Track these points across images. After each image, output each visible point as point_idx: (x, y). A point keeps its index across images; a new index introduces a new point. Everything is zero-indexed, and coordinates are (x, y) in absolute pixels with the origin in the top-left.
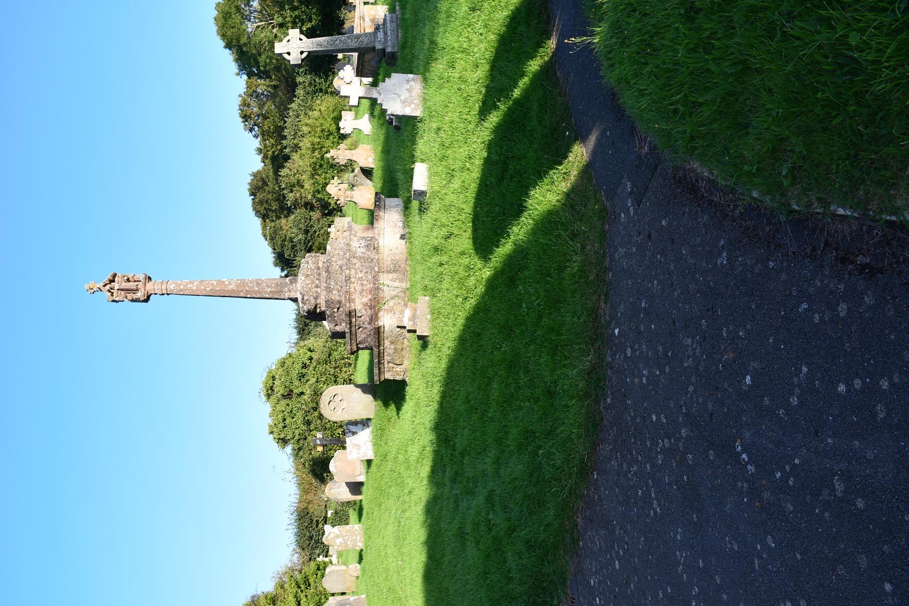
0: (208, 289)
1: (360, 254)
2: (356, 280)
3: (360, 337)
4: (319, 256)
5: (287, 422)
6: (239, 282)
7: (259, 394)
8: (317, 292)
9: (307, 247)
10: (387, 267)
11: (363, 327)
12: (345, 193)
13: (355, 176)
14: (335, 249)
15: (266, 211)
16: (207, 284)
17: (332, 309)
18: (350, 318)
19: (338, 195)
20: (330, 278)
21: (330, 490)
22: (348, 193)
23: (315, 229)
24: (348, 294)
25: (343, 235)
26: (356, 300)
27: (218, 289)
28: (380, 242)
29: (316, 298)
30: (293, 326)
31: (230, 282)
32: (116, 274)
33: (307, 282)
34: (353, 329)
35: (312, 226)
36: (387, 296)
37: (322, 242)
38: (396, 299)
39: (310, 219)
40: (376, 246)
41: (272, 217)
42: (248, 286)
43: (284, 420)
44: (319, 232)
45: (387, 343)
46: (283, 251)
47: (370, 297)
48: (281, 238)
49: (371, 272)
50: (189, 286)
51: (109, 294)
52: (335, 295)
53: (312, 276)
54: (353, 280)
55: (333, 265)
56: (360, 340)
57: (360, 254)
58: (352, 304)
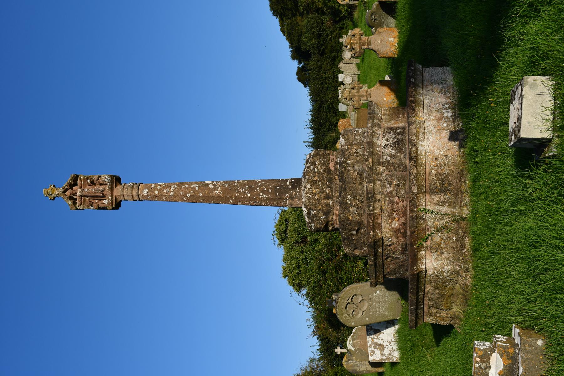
0: (188, 195)
1: (389, 159)
2: (383, 196)
3: (388, 267)
4: (329, 154)
5: (302, 269)
6: (226, 185)
7: (272, 237)
8: (327, 205)
9: (319, 51)
10: (430, 185)
11: (392, 257)
12: (360, 39)
13: (372, 15)
14: (352, 145)
15: (283, 10)
16: (187, 188)
17: (349, 232)
18: (375, 249)
19: (351, 43)
20: (345, 189)
21: (348, 361)
22: (365, 38)
23: (327, 32)
24: (372, 217)
25: (360, 93)
26: (384, 224)
27: (201, 195)
28: (420, 148)
29: (327, 213)
30: (309, 126)
31: (215, 186)
32: (78, 176)
33: (314, 191)
34: (380, 260)
35: (324, 30)
36: (431, 228)
37: (334, 45)
38: (445, 231)
39: (322, 23)
40: (414, 155)
41: (288, 15)
42: (239, 191)
43: (299, 267)
44: (331, 35)
45: (428, 288)
46: (300, 45)
47: (403, 220)
48: (297, 33)
49: (404, 185)
50: (165, 191)
51: (70, 202)
52: (353, 214)
53: (320, 183)
54: (378, 197)
55: (349, 171)
56: (388, 271)
57: (389, 159)
58: (378, 231)
